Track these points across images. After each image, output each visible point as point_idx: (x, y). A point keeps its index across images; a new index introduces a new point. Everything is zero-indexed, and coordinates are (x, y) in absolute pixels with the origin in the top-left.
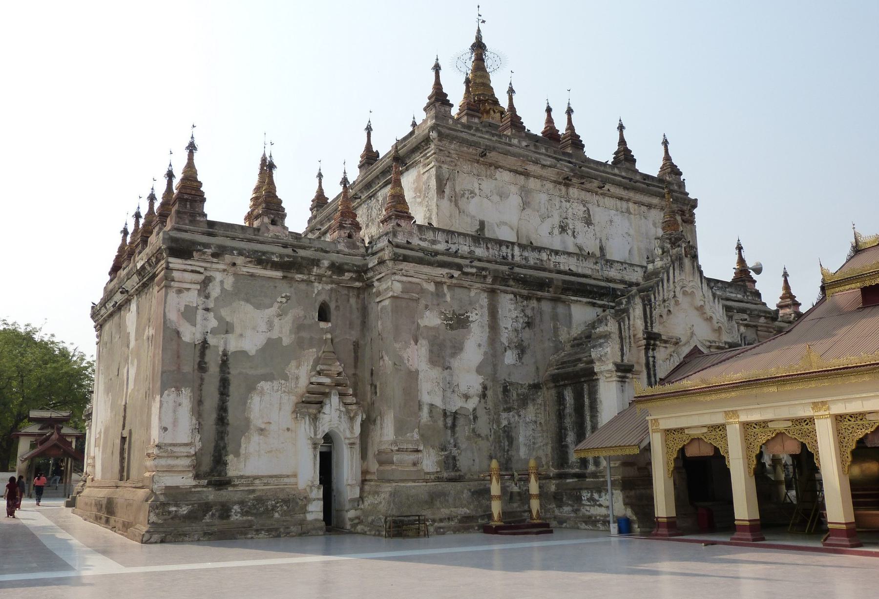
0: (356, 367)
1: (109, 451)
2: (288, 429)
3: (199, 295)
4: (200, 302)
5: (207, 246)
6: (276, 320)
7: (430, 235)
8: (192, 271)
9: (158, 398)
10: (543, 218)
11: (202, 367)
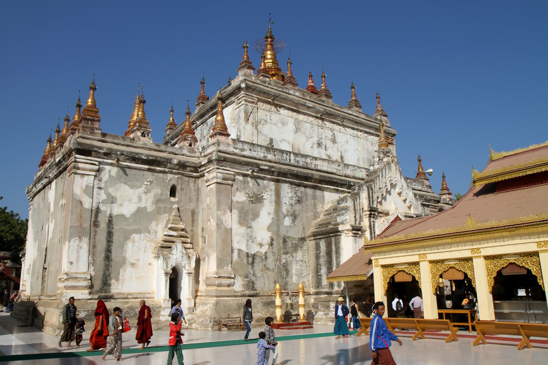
0: (193, 226)
10: (308, 138)
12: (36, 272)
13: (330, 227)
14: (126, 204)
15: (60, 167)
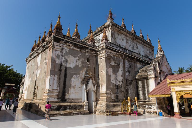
0: (94, 73)
1: (30, 92)
2: (80, 87)
3: (60, 52)
4: (61, 54)
5: (63, 40)
6: (78, 60)
7: (112, 45)
8: (59, 46)
9: (49, 77)
10: (130, 46)
11: (60, 70)
12: (30, 90)
13: (143, 76)
14: (72, 63)
15: (44, 48)
